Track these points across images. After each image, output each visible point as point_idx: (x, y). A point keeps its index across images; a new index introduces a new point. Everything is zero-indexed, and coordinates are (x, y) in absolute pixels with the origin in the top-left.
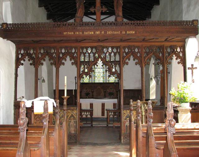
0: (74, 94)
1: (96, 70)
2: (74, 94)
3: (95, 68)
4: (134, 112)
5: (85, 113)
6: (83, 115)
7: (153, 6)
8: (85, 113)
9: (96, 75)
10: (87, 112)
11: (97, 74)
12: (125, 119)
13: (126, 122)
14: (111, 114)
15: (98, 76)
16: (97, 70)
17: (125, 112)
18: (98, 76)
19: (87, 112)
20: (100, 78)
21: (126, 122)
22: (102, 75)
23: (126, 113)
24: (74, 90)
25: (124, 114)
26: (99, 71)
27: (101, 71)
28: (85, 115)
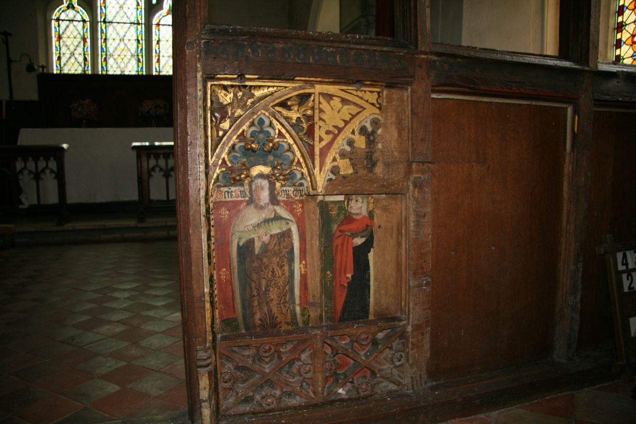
0: (4, 114)
1: (110, 29)
2: (4, 114)
3: (105, 22)
4: (329, 97)
5: (31, 165)
6: (21, 171)
7: (151, 201)
8: (31, 165)
9: (111, 50)
10: (36, 160)
11: (115, 44)
12: (233, 177)
13: (234, 207)
14: (157, 165)
15: (118, 52)
16: (114, 28)
17: (226, 98)
18: (118, 52)
19: (36, 160)
20: (126, 60)
21: (234, 207)
22: (133, 50)
23: (238, 103)
24: (7, 101)
25: (221, 110)
26: (122, 35)
27: (128, 36)
28: (161, 170)
